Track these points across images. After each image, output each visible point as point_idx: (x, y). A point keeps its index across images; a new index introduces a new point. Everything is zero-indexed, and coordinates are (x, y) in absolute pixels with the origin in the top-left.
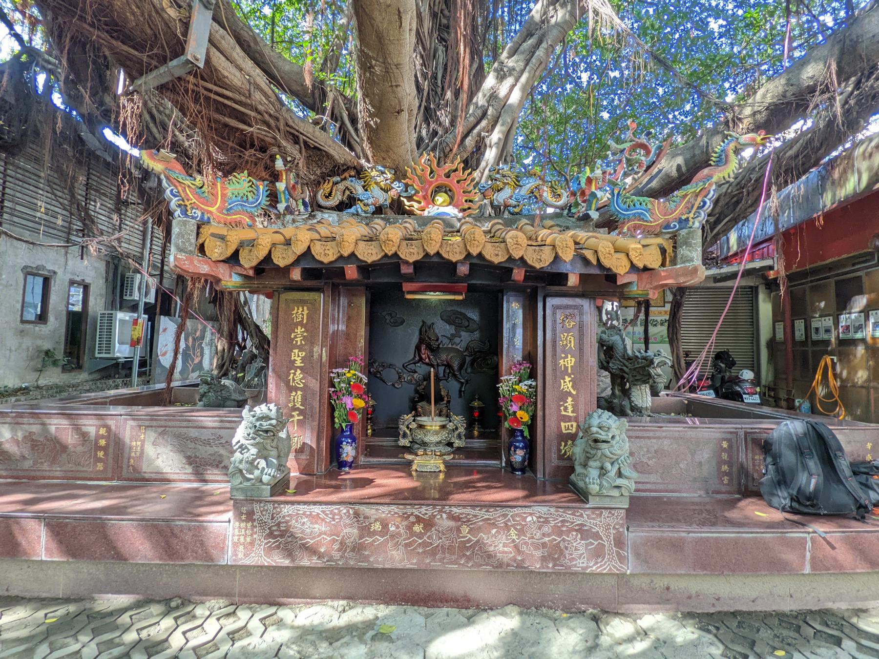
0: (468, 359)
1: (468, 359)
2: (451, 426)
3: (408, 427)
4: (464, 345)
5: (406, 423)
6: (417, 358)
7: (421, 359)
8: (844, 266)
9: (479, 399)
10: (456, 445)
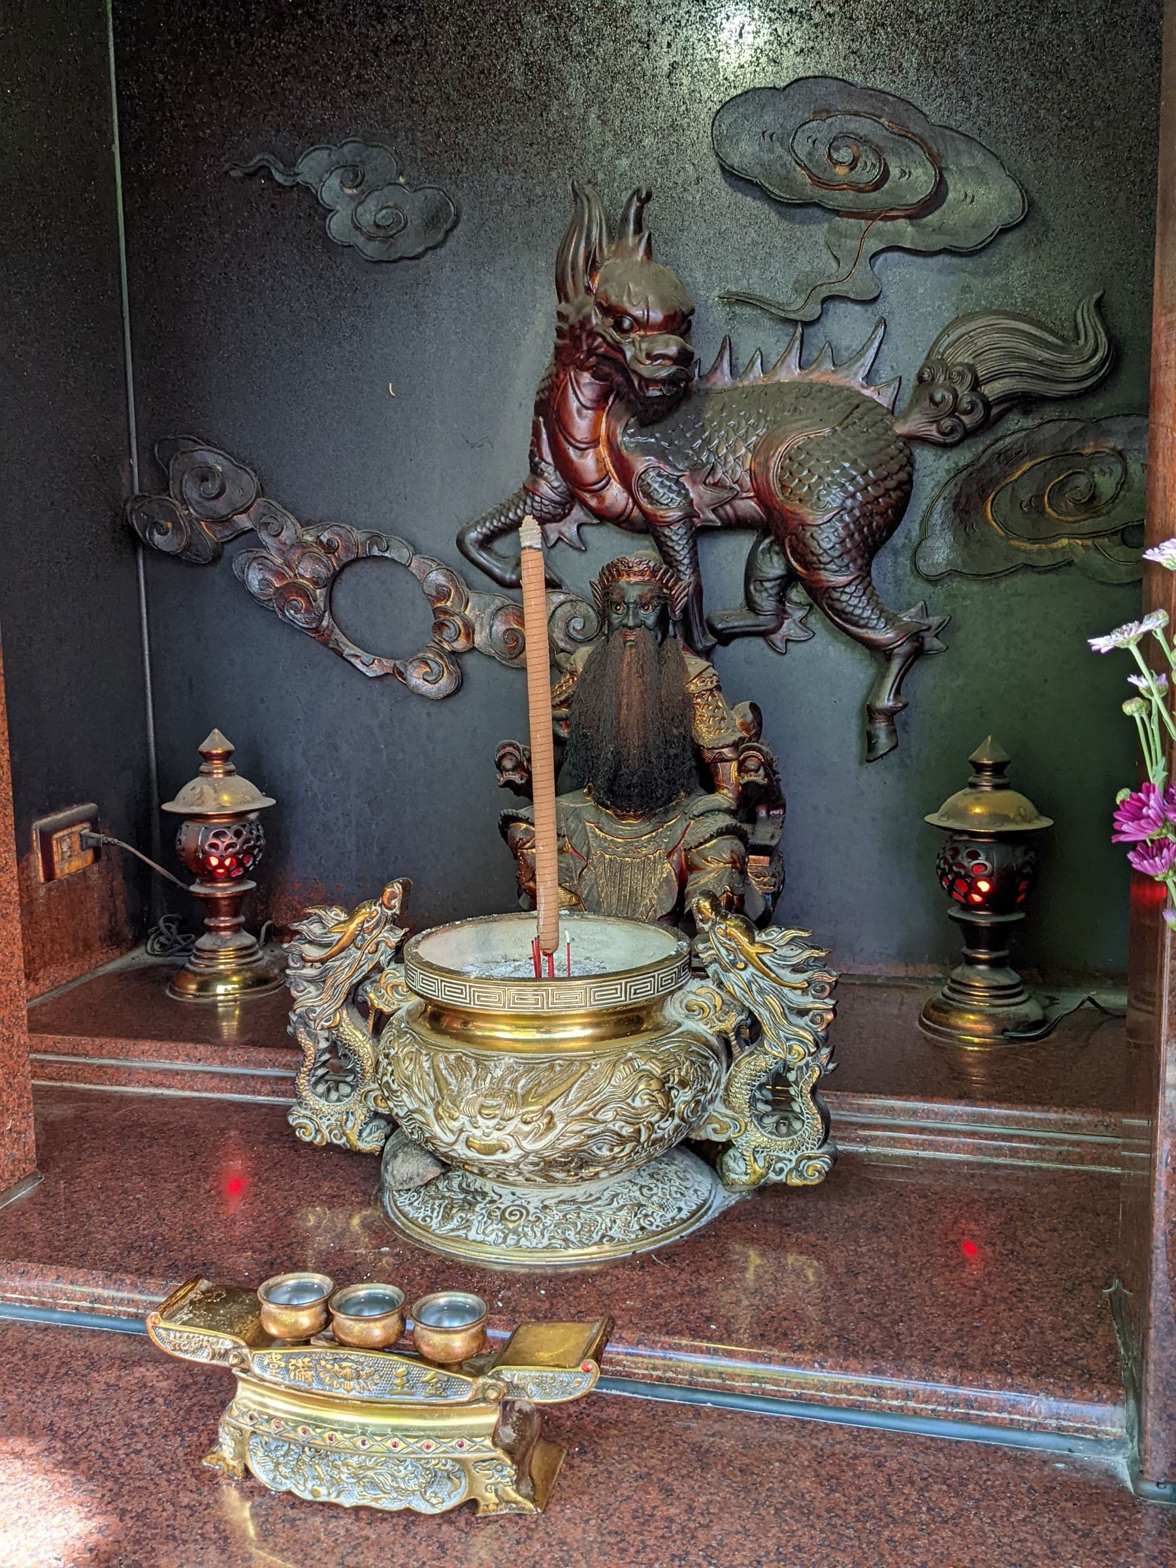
0: (933, 470)
1: (933, 470)
2: (696, 1011)
3: (355, 1000)
4: (906, 358)
5: (345, 973)
6: (551, 486)
7: (576, 488)
8: (1028, 1151)
9: (1002, 774)
10: (742, 1170)
